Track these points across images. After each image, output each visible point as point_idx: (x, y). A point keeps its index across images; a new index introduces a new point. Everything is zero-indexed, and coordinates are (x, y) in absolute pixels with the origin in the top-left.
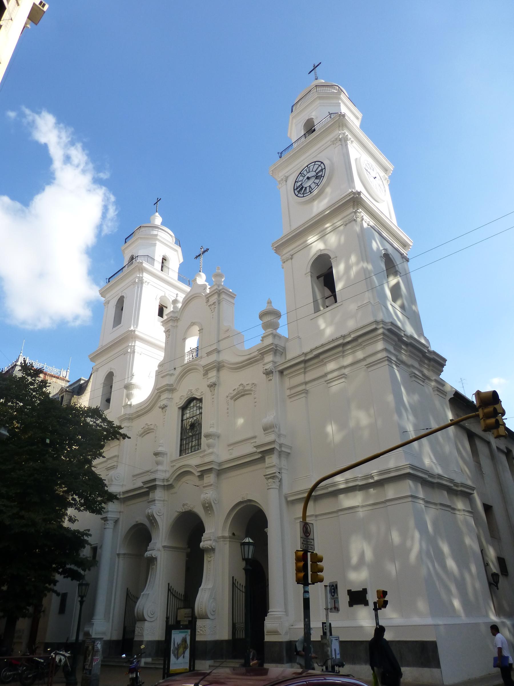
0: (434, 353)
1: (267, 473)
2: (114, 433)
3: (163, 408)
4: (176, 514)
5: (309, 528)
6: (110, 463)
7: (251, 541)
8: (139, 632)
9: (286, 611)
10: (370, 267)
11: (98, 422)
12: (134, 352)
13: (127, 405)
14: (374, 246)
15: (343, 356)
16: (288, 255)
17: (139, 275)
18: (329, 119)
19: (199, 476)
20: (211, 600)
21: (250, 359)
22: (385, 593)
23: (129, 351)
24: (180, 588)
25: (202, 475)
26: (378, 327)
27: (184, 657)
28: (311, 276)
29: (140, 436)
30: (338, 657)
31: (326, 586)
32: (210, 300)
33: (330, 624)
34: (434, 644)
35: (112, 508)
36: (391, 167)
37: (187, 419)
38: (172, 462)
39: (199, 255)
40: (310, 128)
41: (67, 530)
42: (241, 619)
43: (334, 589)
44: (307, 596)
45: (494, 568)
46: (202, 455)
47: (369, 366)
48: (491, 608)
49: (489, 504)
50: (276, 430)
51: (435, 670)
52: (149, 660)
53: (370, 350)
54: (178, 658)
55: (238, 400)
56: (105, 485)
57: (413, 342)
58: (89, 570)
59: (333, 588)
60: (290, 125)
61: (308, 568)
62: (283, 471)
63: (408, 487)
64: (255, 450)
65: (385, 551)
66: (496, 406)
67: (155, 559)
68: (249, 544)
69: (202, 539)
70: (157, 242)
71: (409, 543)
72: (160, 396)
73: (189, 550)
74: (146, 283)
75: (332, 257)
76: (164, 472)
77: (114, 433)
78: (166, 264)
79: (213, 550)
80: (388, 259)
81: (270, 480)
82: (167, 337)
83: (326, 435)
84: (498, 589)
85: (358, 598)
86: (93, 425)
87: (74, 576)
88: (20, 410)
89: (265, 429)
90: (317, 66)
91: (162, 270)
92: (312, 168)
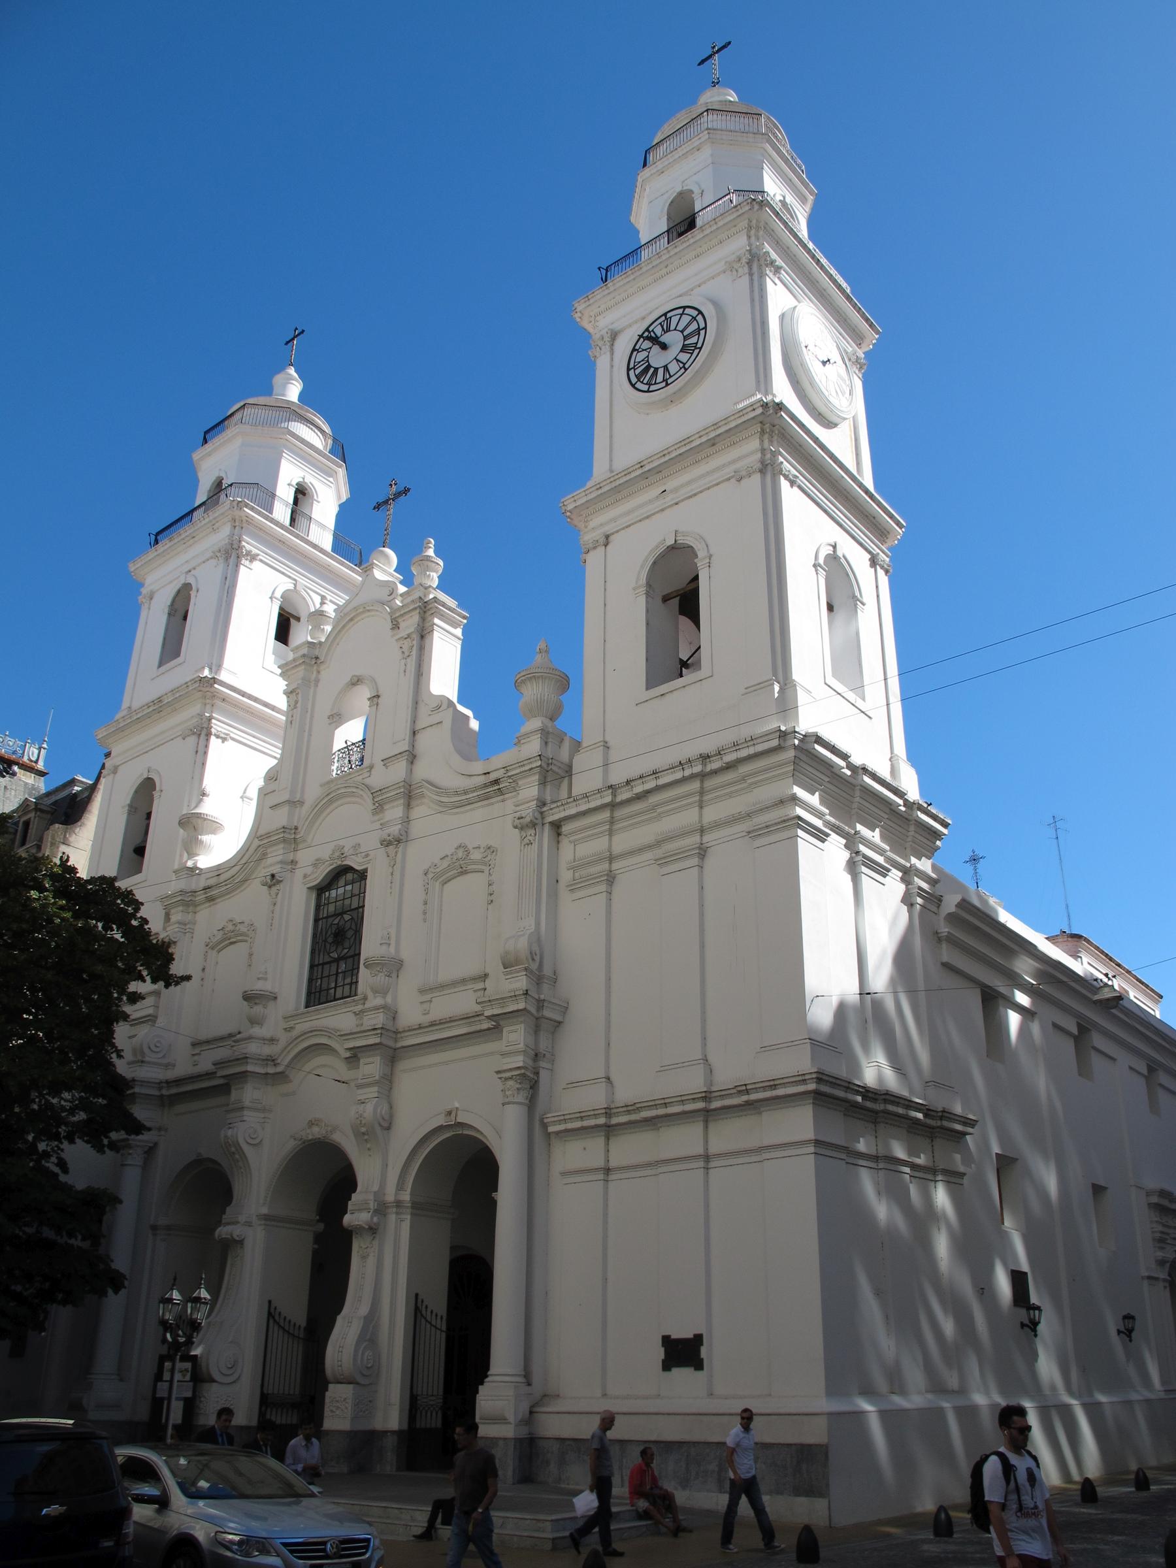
4: (291, 1145)
24: (297, 1312)
25: (354, 1057)
28: (648, 594)
37: (327, 918)
39: (386, 502)
67: (240, 1243)
69: (350, 1207)
73: (321, 1226)
92: (674, 321)
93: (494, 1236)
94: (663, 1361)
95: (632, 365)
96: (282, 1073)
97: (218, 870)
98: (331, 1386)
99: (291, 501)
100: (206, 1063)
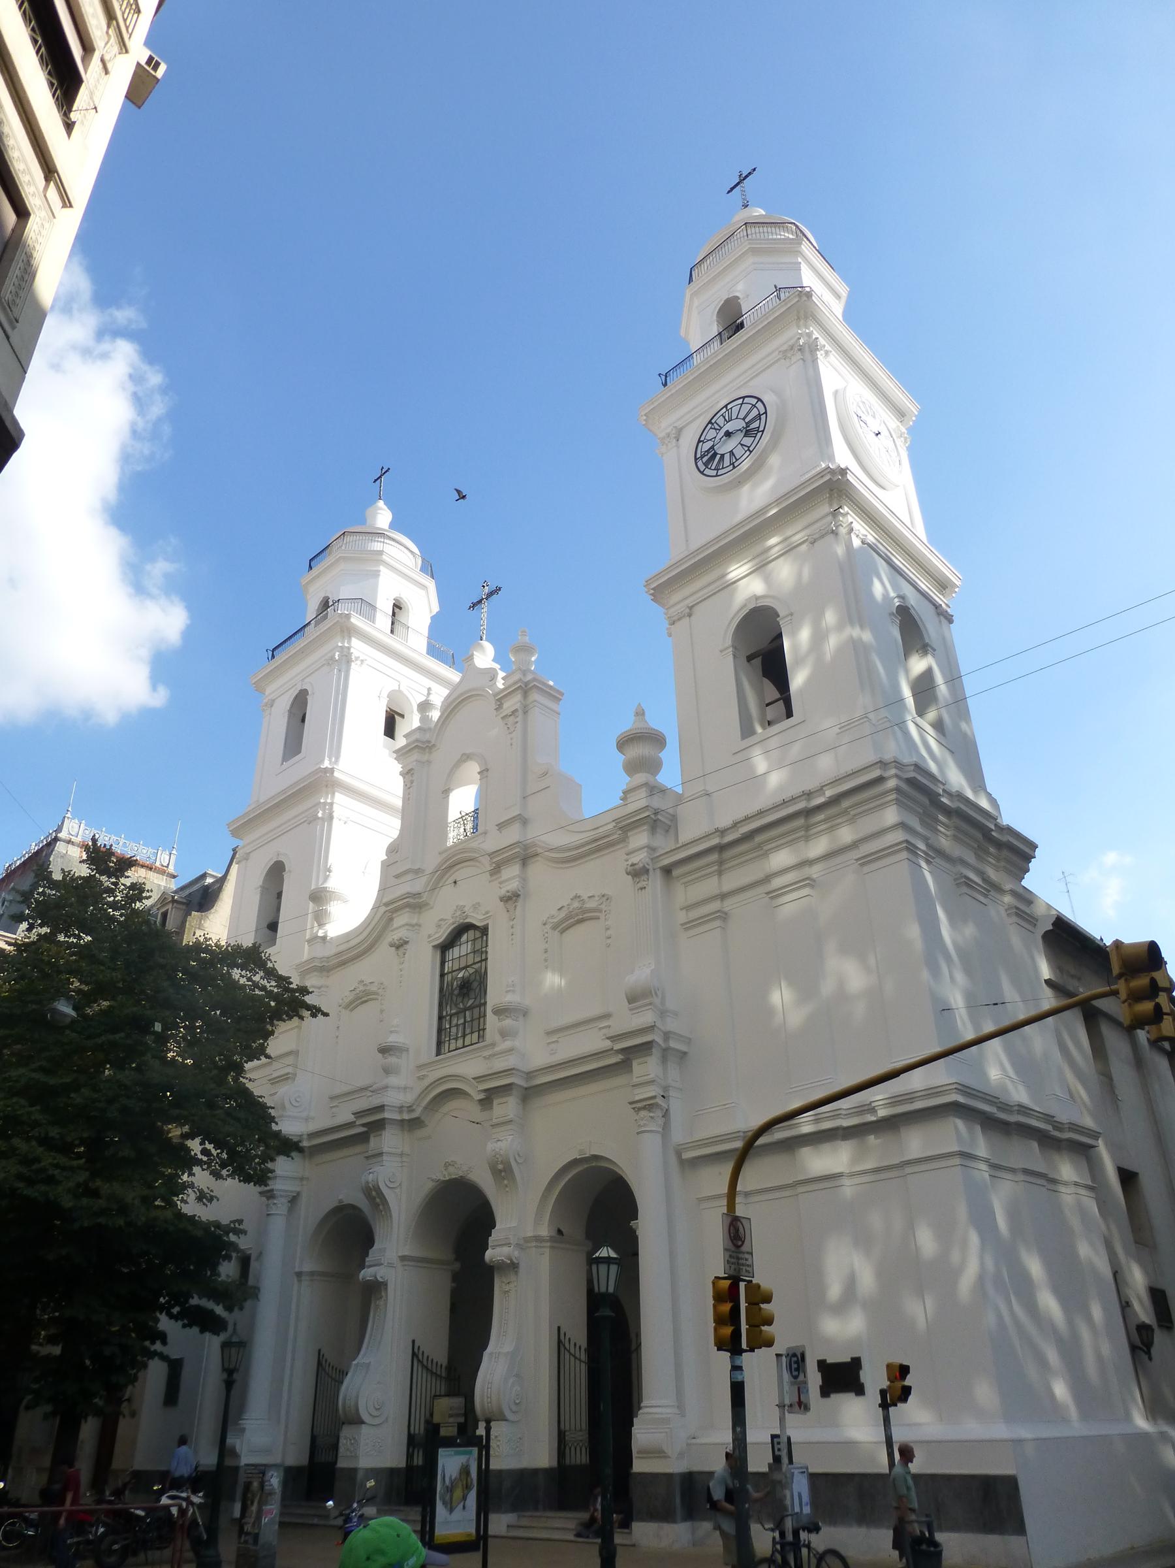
0: (1009, 830)
1: (637, 1098)
2: (292, 1003)
3: (398, 948)
4: (429, 1185)
5: (741, 1230)
6: (277, 1069)
7: (613, 1255)
9: (680, 1406)
10: (867, 636)
11: (257, 978)
12: (331, 818)
13: (317, 937)
14: (878, 589)
15: (807, 838)
16: (681, 607)
17: (343, 642)
18: (776, 302)
19: (480, 1101)
21: (596, 840)
22: (904, 1370)
23: (320, 815)
24: (438, 1353)
25: (489, 1098)
26: (886, 775)
27: (464, 1507)
28: (735, 656)
29: (346, 1008)
30: (807, 1510)
31: (778, 1355)
32: (505, 706)
33: (789, 1439)
34: (1011, 1483)
36: (912, 408)
38: (419, 1067)
39: (480, 602)
40: (732, 323)
41: (191, 1219)
42: (578, 1421)
43: (797, 1362)
44: (740, 1379)
45: (1143, 1312)
46: (486, 1053)
47: (866, 860)
48: (1134, 1400)
49: (1130, 1168)
50: (657, 1001)
51: (1014, 1541)
53: (868, 824)
54: (451, 1510)
55: (571, 931)
56: (272, 1119)
58: (241, 1309)
59: (794, 1359)
60: (686, 309)
61: (739, 1314)
62: (672, 1093)
63: (952, 1134)
64: (607, 1044)
65: (903, 1271)
66: (1157, 975)
68: (608, 1260)
70: (382, 568)
71: (955, 1256)
72: (391, 919)
74: (359, 662)
76: (401, 1091)
77: (292, 1003)
78: (401, 617)
79: (513, 1266)
80: (907, 619)
81: (643, 1113)
82: (408, 787)
83: (769, 1011)
84: (1150, 1359)
85: (842, 1377)
87: (208, 1323)
88: (84, 952)
89: (632, 999)
90: (747, 176)
91: (392, 632)
92: (735, 410)
94: (821, 1388)
96: (418, 1118)
97: (347, 937)
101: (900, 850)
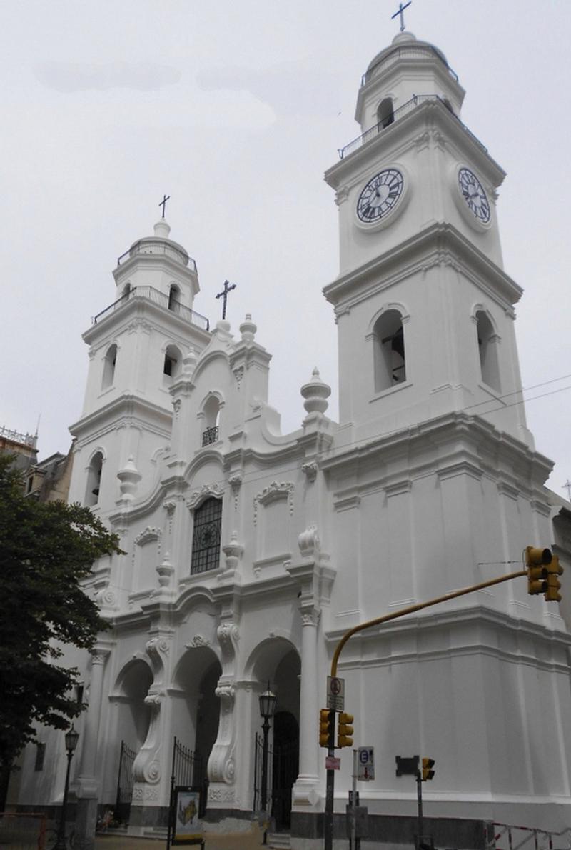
5: (338, 685)
7: (272, 695)
8: (137, 796)
20: (229, 761)
24: (189, 743)
27: (191, 823)
28: (374, 339)
31: (355, 751)
35: (102, 641)
38: (181, 582)
52: (151, 829)
54: (184, 824)
57: (506, 441)
61: (335, 729)
68: (269, 698)
69: (219, 685)
72: (165, 494)
75: (403, 316)
86: (79, 532)
87: (60, 724)
92: (384, 178)
93: (299, 690)
94: (397, 771)
95: (360, 207)
98: (211, 784)
99: (169, 295)
100: (137, 608)
101: (462, 468)
